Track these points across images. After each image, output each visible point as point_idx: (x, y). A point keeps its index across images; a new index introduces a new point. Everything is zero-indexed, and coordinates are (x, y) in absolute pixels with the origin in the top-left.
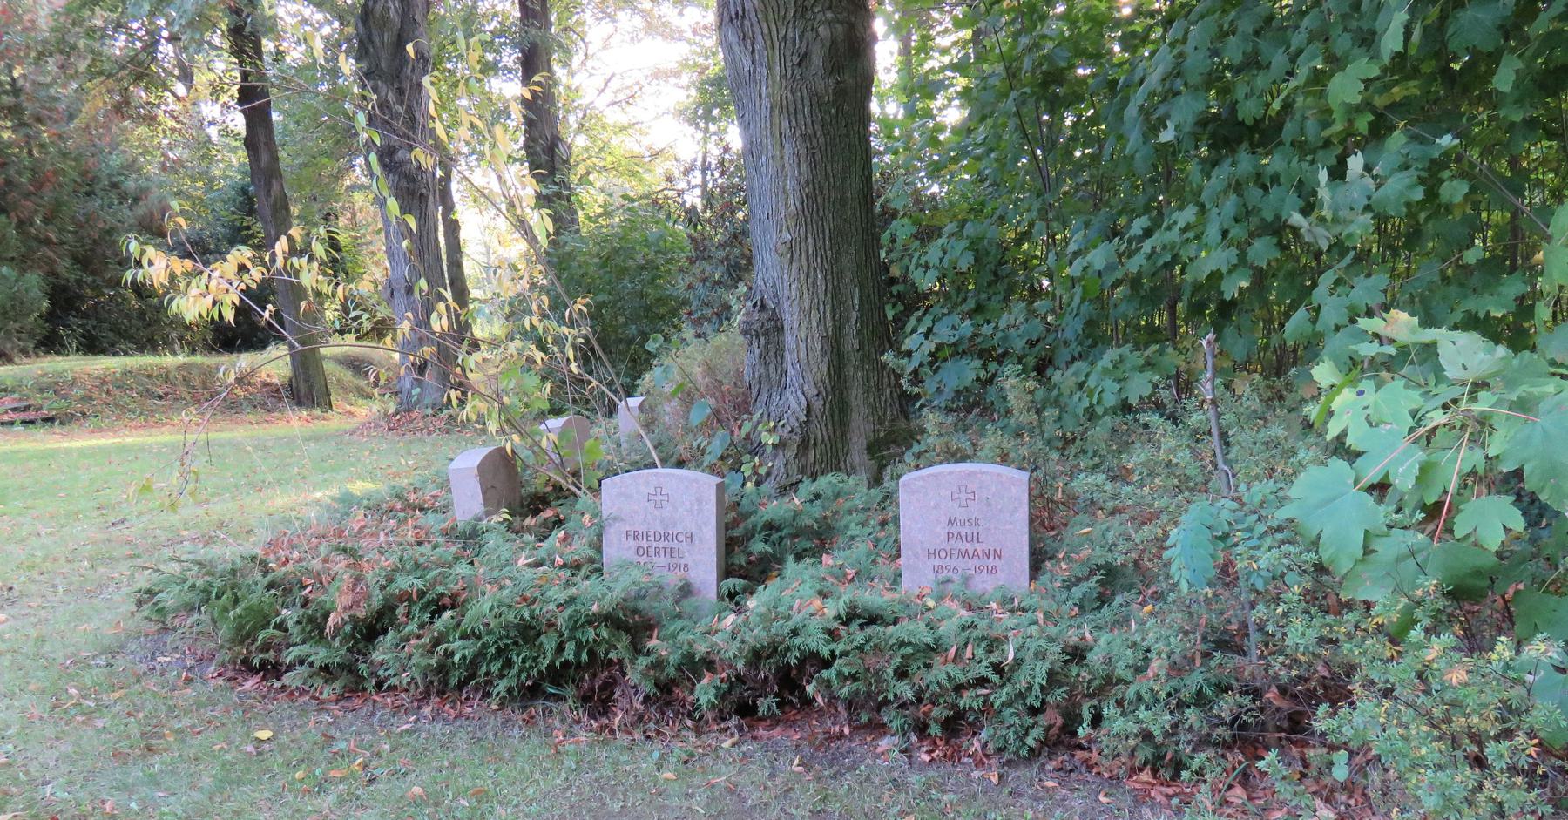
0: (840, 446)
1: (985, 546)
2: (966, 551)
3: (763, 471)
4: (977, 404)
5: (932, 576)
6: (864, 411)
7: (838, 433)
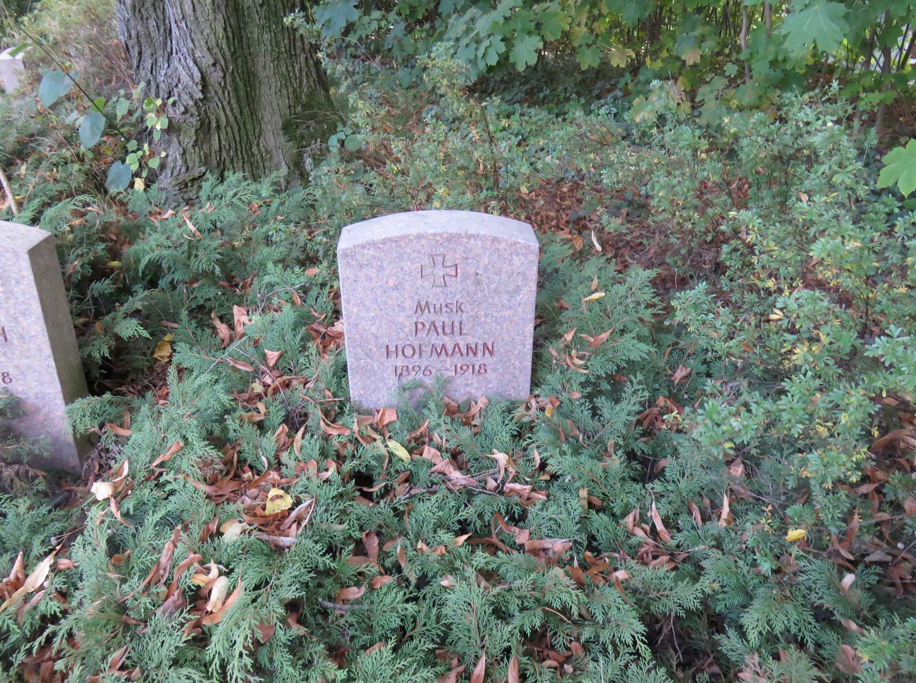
0: (249, 127)
1: (471, 340)
2: (444, 346)
3: (154, 163)
4: (377, 51)
5: (393, 380)
6: (275, 83)
7: (246, 111)
